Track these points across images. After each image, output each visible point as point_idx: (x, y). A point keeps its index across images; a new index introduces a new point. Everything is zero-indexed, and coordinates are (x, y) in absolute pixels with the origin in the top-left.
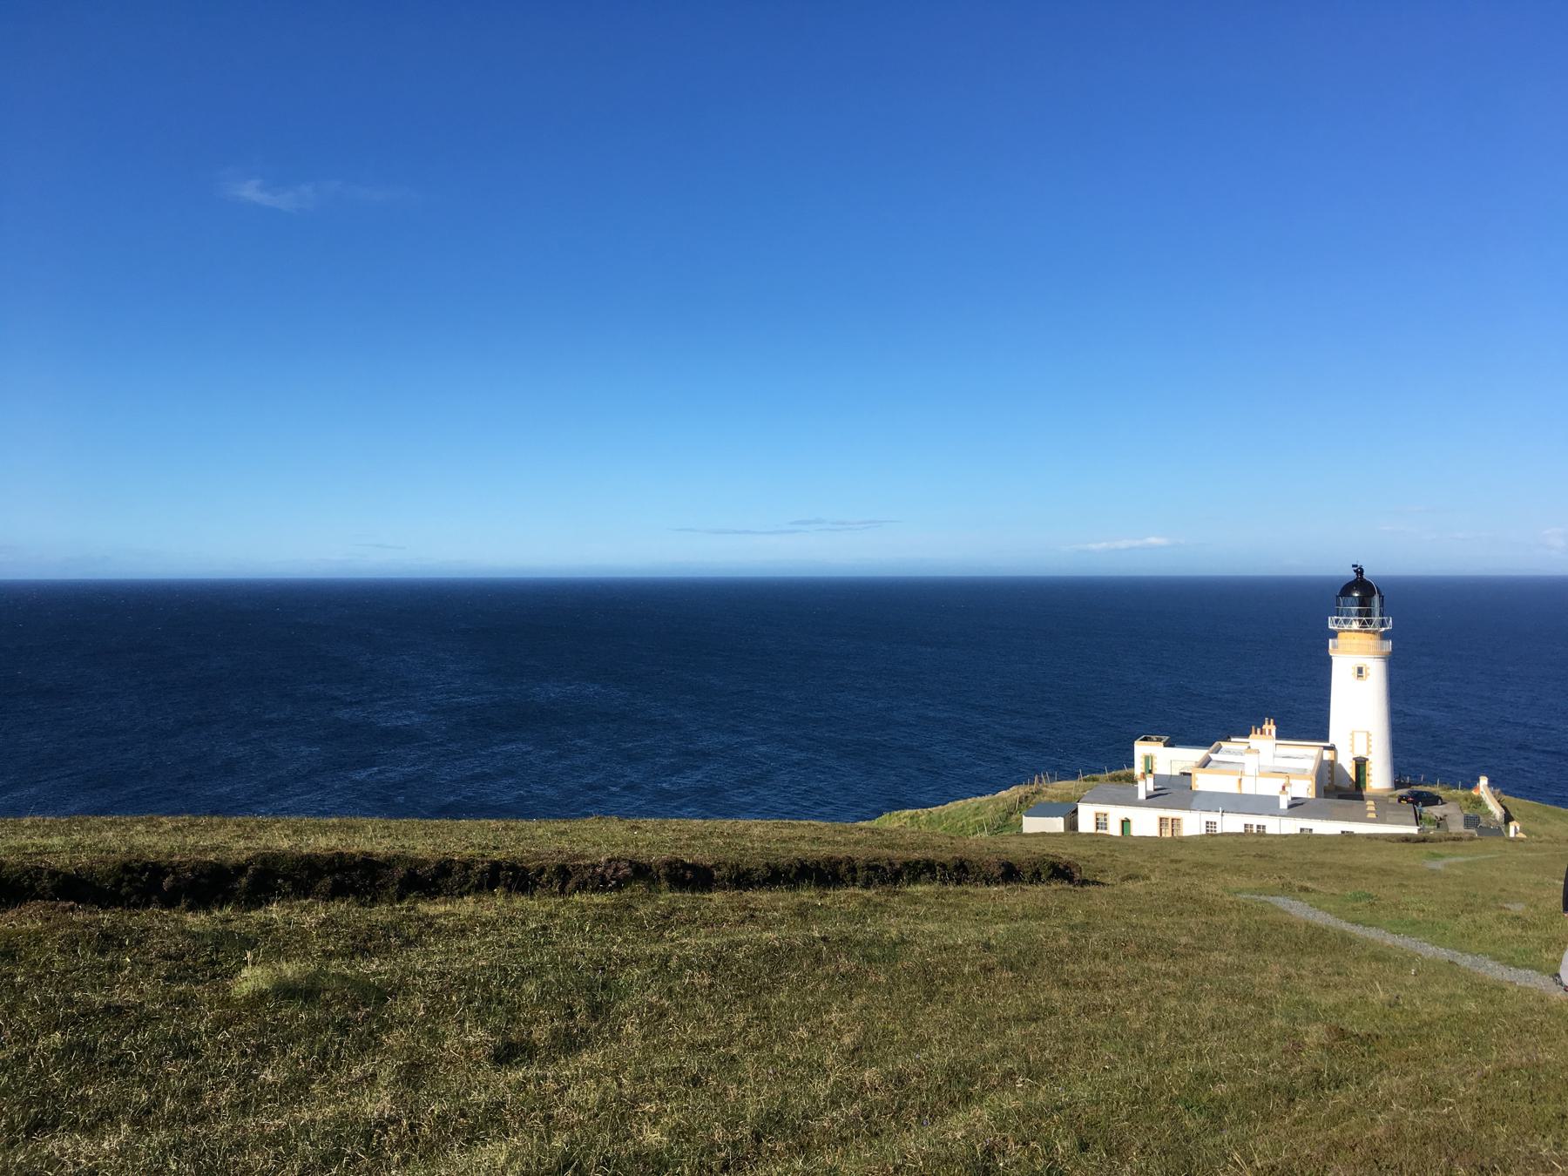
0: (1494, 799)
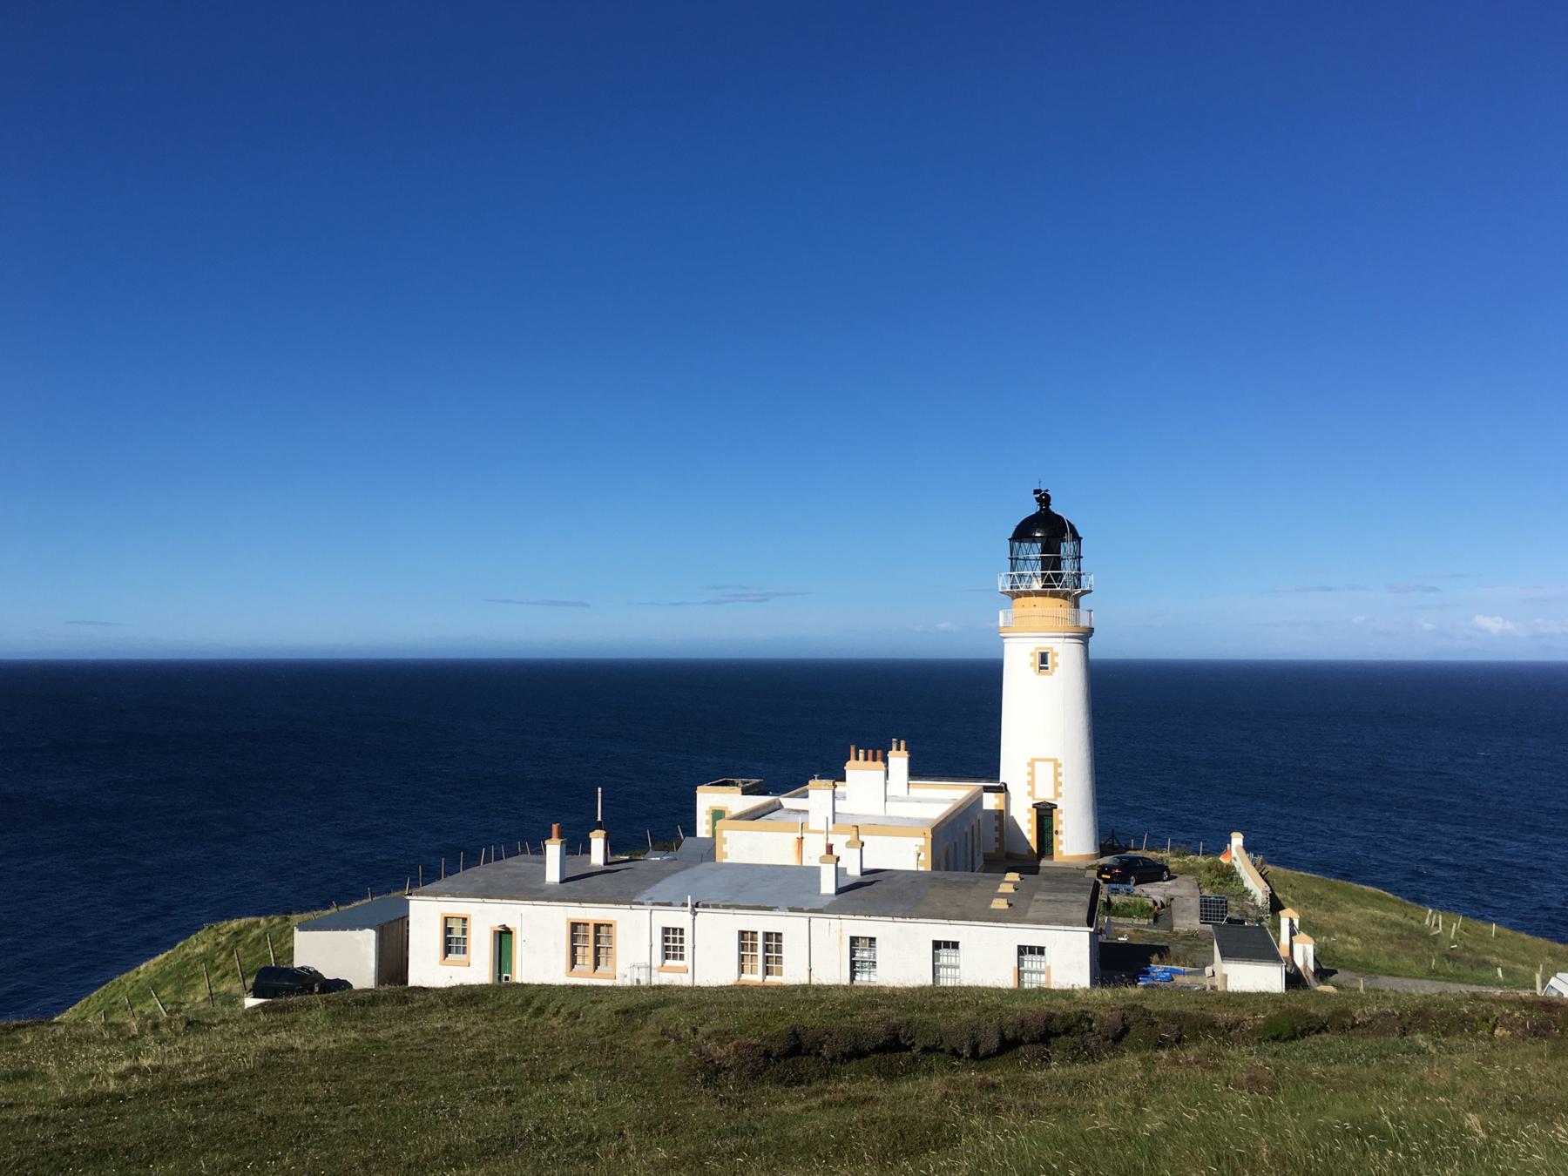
0: (1253, 869)
